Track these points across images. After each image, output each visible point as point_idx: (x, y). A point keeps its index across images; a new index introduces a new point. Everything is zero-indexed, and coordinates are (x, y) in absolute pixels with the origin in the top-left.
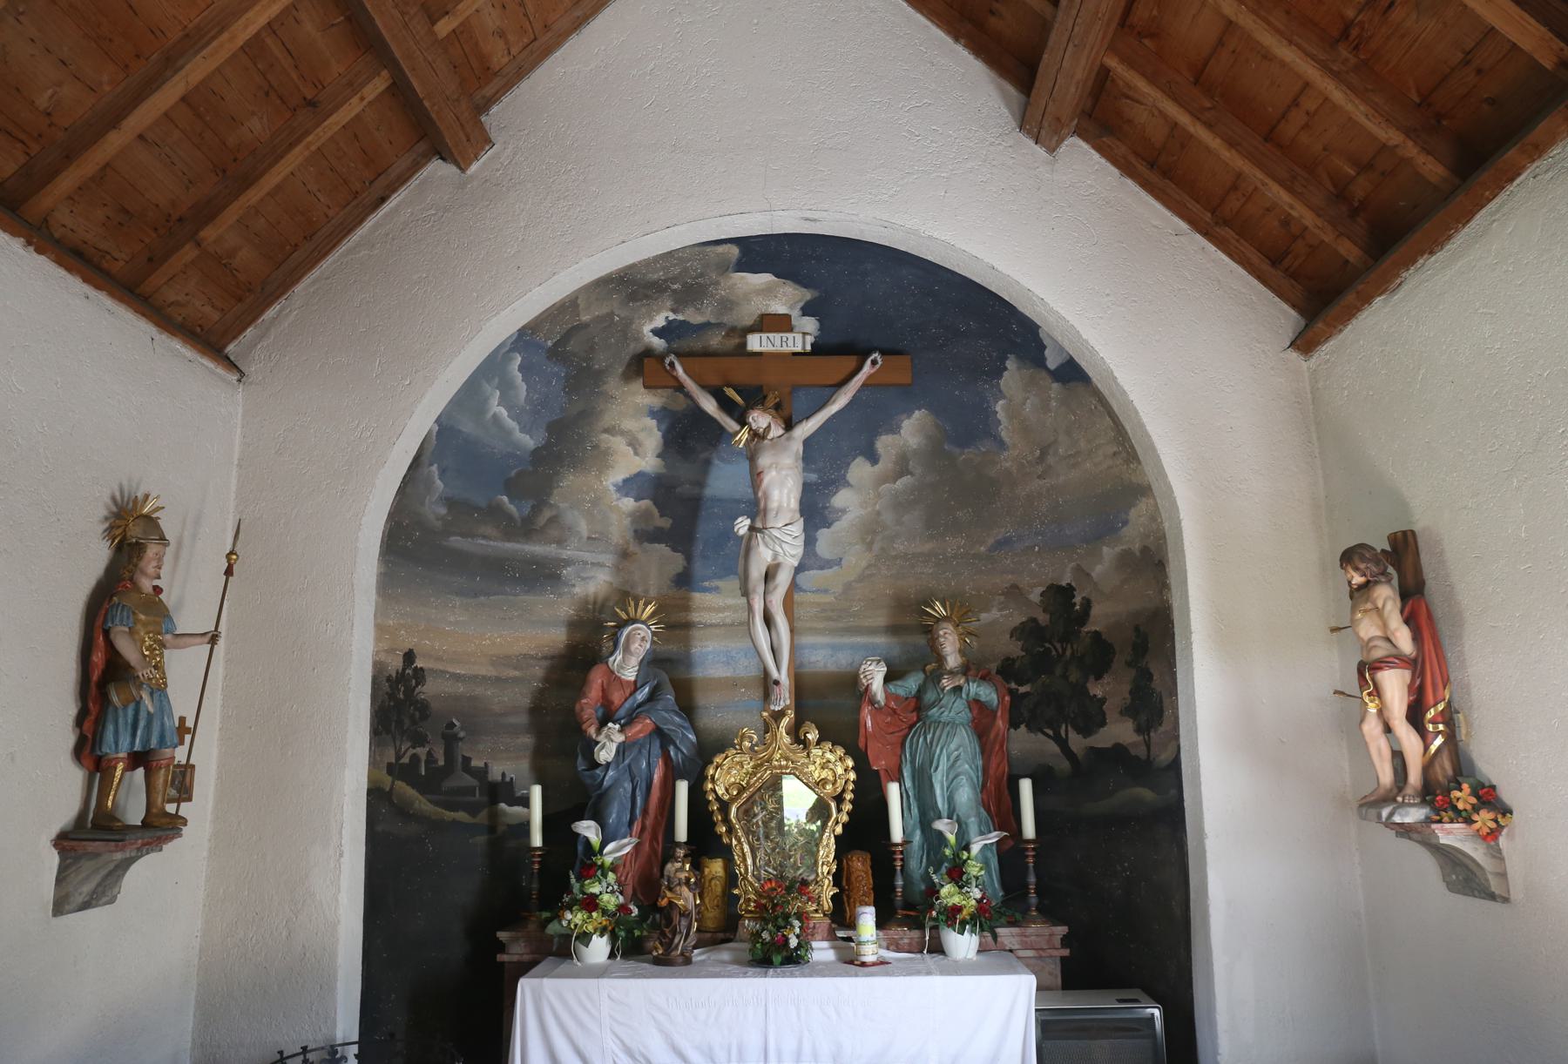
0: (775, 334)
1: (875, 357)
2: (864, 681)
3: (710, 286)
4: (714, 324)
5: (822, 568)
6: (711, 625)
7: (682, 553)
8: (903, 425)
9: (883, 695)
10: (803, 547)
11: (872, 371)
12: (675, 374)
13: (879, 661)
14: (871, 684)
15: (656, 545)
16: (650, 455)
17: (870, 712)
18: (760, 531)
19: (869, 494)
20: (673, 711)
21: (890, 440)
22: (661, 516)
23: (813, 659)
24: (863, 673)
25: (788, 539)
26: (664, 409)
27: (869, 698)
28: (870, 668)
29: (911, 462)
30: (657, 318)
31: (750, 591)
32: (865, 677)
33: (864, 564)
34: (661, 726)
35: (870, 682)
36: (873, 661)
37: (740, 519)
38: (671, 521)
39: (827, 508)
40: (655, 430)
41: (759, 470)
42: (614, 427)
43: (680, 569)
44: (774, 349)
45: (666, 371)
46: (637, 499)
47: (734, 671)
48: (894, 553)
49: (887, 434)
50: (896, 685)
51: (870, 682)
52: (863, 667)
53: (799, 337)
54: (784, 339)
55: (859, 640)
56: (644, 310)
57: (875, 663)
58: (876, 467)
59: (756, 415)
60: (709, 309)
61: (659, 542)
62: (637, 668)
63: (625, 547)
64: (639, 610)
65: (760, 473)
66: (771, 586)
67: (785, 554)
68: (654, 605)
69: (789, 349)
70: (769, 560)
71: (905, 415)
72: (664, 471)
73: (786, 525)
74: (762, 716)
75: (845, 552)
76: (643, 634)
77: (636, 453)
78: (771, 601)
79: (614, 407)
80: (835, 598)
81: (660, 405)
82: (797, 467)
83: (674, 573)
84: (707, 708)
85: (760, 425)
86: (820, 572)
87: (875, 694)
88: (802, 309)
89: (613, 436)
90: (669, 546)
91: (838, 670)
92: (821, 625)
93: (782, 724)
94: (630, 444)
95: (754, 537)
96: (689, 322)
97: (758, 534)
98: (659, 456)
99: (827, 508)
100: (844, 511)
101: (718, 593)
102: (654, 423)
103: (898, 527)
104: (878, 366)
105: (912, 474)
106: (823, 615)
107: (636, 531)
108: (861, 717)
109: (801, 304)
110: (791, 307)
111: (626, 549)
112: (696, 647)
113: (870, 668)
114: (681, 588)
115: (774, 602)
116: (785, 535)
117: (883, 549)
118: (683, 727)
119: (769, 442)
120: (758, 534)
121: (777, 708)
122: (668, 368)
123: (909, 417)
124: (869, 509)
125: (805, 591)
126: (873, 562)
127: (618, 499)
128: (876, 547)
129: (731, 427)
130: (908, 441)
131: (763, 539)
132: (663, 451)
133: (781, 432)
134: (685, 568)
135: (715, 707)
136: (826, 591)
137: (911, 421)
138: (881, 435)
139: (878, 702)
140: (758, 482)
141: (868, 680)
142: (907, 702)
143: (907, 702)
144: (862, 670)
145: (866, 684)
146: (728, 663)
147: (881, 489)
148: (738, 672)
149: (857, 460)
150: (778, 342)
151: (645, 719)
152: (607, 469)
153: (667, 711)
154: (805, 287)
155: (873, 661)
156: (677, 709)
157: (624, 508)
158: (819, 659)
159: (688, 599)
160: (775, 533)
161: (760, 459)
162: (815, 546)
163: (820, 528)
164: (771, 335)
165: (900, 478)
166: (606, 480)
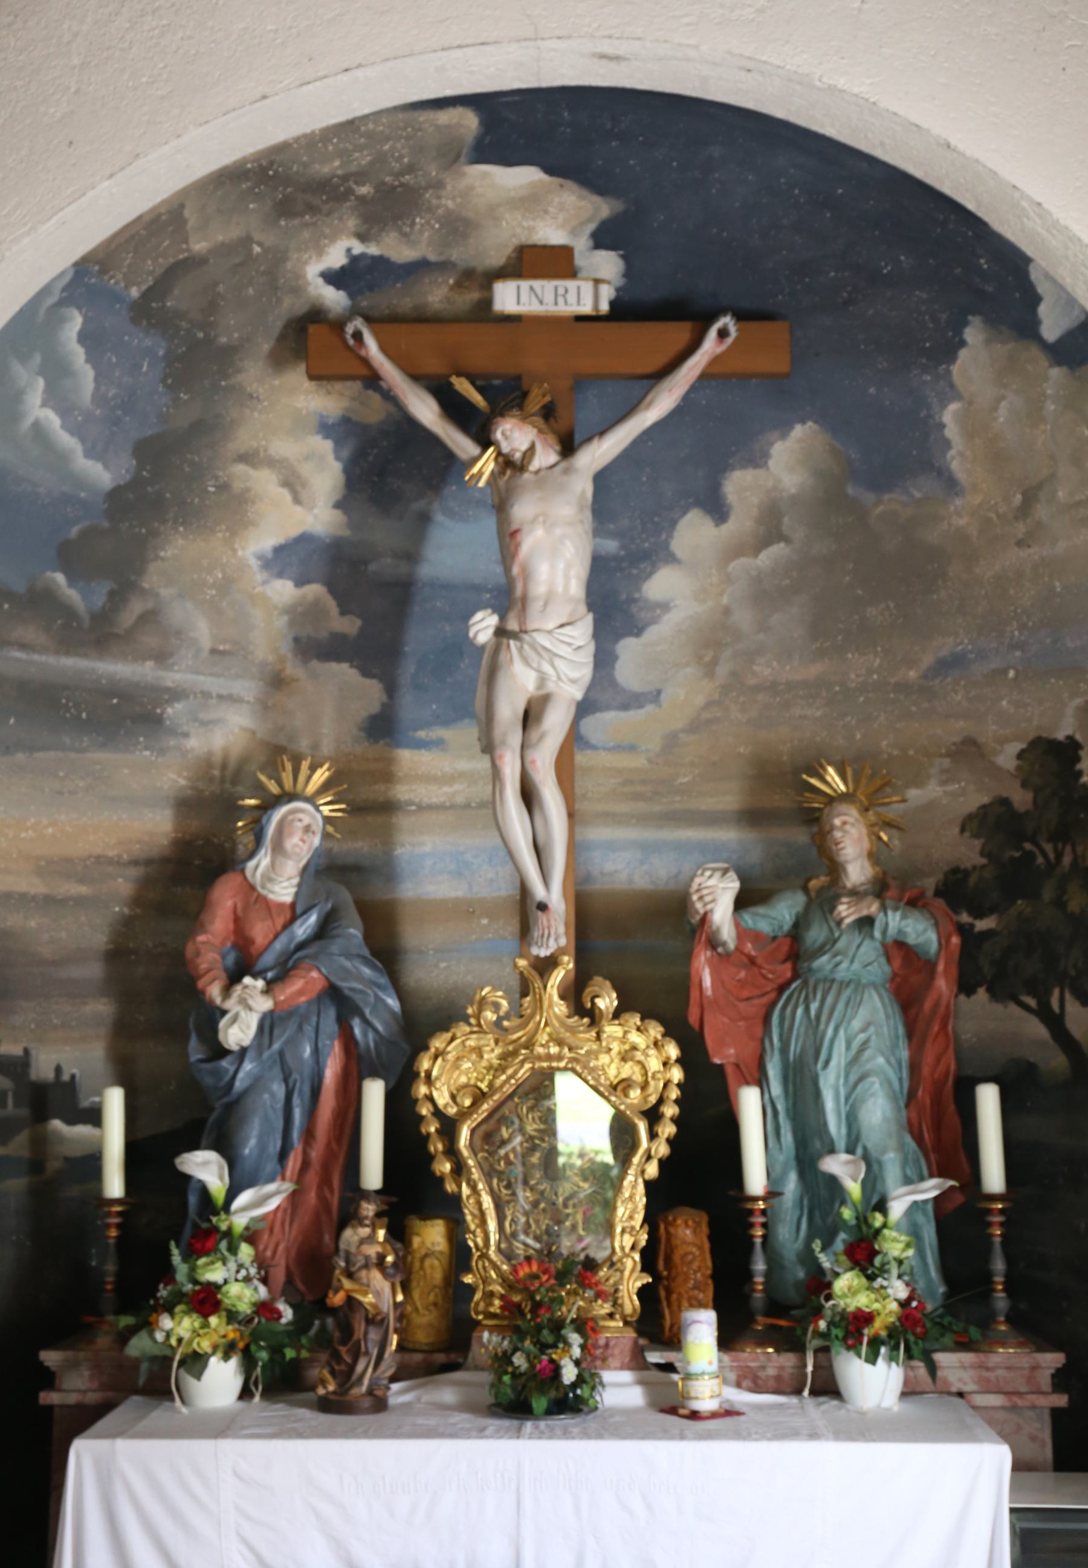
2: (699, 906)
3: (426, 189)
5: (625, 707)
6: (431, 808)
7: (381, 680)
12: (363, 353)
13: (725, 872)
14: (711, 911)
22: (343, 613)
23: (609, 867)
24: (698, 890)
25: (563, 650)
26: (346, 421)
29: (786, 520)
32: (701, 898)
33: (700, 700)
37: (479, 616)
38: (358, 623)
40: (331, 458)
41: (514, 527)
42: (256, 453)
43: (375, 708)
46: (299, 583)
48: (752, 682)
49: (743, 467)
50: (757, 914)
51: (709, 907)
52: (697, 880)
54: (561, 291)
56: (306, 234)
57: (718, 874)
60: (426, 234)
64: (302, 778)
66: (534, 735)
67: (559, 678)
68: (329, 769)
73: (562, 626)
74: (515, 966)
76: (307, 820)
77: (297, 500)
79: (256, 414)
80: (650, 761)
83: (364, 714)
86: (623, 715)
87: (718, 930)
89: (254, 466)
90: (356, 667)
92: (622, 808)
94: (287, 484)
95: (504, 647)
97: (512, 642)
98: (338, 505)
99: (635, 601)
100: (665, 607)
102: (326, 446)
103: (761, 636)
104: (729, 341)
107: (297, 640)
109: (592, 227)
110: (574, 232)
115: (539, 763)
117: (733, 674)
118: (379, 986)
121: (543, 953)
122: (351, 342)
123: (784, 436)
124: (710, 603)
125: (594, 748)
126: (716, 697)
131: (520, 650)
133: (553, 457)
134: (384, 705)
135: (436, 951)
136: (632, 748)
139: (724, 944)
140: (512, 548)
141: (705, 905)
142: (774, 945)
143: (774, 945)
145: (702, 911)
150: (549, 297)
151: (310, 970)
153: (348, 956)
155: (714, 870)
156: (366, 952)
159: (390, 761)
160: (542, 640)
162: (613, 668)
164: (537, 284)
166: (243, 548)
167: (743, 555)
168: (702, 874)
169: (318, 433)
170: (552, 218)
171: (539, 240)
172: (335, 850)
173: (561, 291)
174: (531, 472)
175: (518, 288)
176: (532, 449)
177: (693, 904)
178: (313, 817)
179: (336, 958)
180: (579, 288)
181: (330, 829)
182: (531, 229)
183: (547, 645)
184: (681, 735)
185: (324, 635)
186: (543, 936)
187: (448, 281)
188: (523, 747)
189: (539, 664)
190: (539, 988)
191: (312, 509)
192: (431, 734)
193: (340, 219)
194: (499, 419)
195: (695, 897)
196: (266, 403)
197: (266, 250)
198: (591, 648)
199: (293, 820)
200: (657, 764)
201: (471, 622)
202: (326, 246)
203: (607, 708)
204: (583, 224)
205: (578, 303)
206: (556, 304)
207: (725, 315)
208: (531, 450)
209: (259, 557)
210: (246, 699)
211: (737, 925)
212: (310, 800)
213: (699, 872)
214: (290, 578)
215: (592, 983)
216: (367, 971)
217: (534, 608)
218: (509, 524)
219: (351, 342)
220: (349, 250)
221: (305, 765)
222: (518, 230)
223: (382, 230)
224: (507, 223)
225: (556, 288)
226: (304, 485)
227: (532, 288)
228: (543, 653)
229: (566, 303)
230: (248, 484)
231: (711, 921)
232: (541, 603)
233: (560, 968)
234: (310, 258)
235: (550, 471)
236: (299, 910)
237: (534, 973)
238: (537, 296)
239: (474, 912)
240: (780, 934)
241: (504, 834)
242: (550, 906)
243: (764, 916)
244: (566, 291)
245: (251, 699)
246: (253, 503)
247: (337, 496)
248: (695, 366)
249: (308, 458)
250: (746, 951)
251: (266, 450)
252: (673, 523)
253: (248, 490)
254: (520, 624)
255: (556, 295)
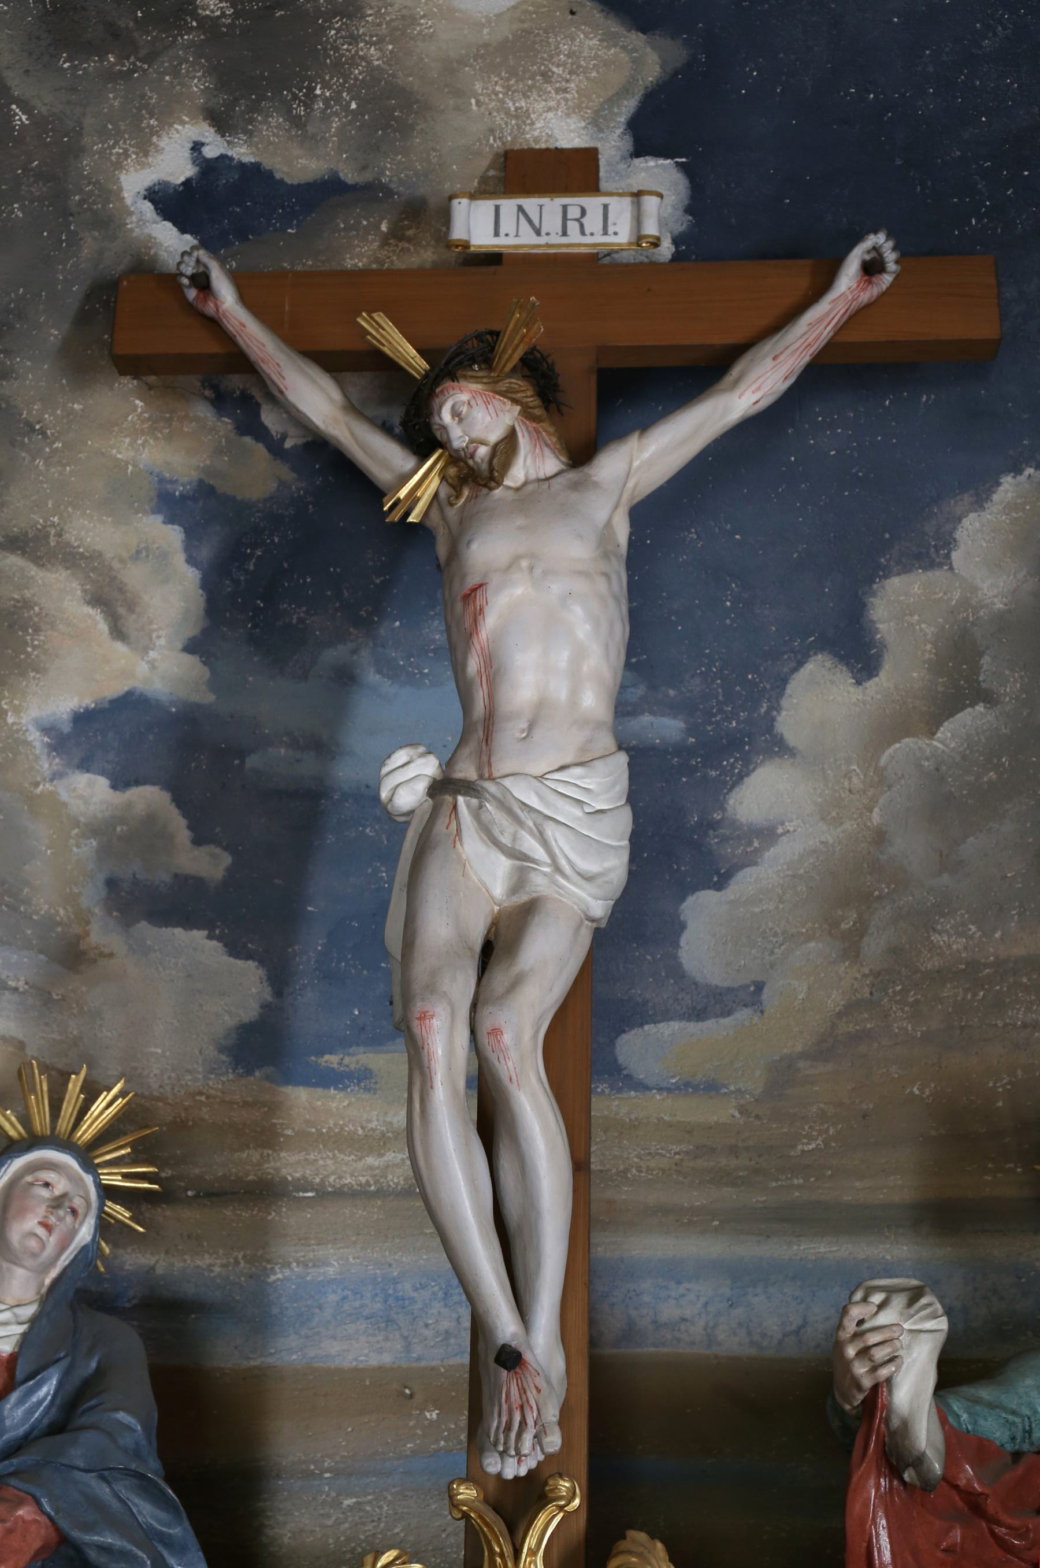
0: (545, 201)
1: (875, 249)
2: (860, 1369)
3: (329, 16)
4: (354, 188)
5: (698, 1014)
6: (341, 1194)
7: (262, 963)
8: (960, 534)
9: (939, 1438)
10: (625, 857)
11: (865, 297)
12: (210, 309)
13: (915, 1295)
14: (889, 1381)
15: (178, 931)
16: (162, 642)
17: (887, 1501)
18: (468, 788)
19: (847, 775)
20: (128, 1472)
21: (916, 589)
22: (197, 842)
23: (669, 1312)
24: (857, 1336)
25: (567, 813)
26: (205, 491)
27: (882, 1445)
28: (883, 1319)
29: (986, 660)
30: (163, 142)
31: (417, 987)
32: (864, 1352)
33: (835, 1000)
34: (76, 1534)
35: (884, 1372)
36: (891, 1291)
37: (401, 757)
38: (227, 859)
39: (714, 825)
40: (179, 559)
41: (471, 581)
42: (42, 536)
43: (250, 1012)
44: (542, 240)
45: (190, 308)
46: (119, 783)
47: (408, 1348)
48: (933, 963)
49: (906, 570)
50: (977, 1401)
51: (884, 1372)
52: (856, 1312)
53: (621, 210)
54: (574, 213)
55: (823, 1249)
56: (114, 100)
57: (899, 1301)
58: (872, 684)
59: (464, 397)
60: (335, 124)
61: (188, 922)
62: (29, 1311)
63: (75, 929)
64: (68, 1110)
65: (475, 590)
66: (499, 979)
67: (558, 869)
68: (122, 1094)
69: (588, 240)
70: (499, 890)
71: (967, 498)
72: (210, 698)
73: (562, 768)
74: (454, 1504)
75: (772, 966)
76: (61, 1185)
77: (118, 633)
78: (496, 1032)
79: (40, 463)
80: (743, 1110)
81: (195, 475)
82: (606, 575)
83: (230, 1021)
84: (309, 1475)
85: (477, 433)
86: (693, 1027)
87: (906, 1426)
88: (634, 125)
89: (38, 561)
90: (219, 939)
91: (752, 1352)
92: (696, 1198)
93: (530, 1541)
94: (97, 600)
95: (446, 809)
96: (269, 175)
97: (461, 799)
98: (191, 647)
99: (714, 825)
100: (768, 834)
101: (367, 1090)
102: (173, 536)
103: (945, 879)
104: (886, 280)
105: (988, 698)
106: (700, 1163)
107: (112, 883)
108: (851, 1524)
109: (629, 106)
110: (597, 122)
111: (79, 938)
112: (287, 1265)
113: (883, 1319)
114: (249, 1072)
115: (507, 1038)
116: (561, 803)
117: (894, 951)
118: (167, 1541)
119: (510, 495)
120: (461, 799)
121: (512, 1469)
122: (192, 294)
123: (980, 502)
124: (849, 826)
125: (642, 1087)
126: (866, 993)
127: (56, 776)
128: (874, 946)
129: (385, 464)
130: (975, 589)
131: (477, 814)
132: (205, 632)
133: (551, 464)
134: (265, 1006)
135: (337, 1473)
136: (712, 1088)
137: (986, 516)
138: (886, 577)
139: (919, 1462)
140: (468, 623)
141: (874, 1369)
142: (1020, 1470)
143: (1020, 1470)
144: (850, 1327)
145: (867, 1383)
146: (389, 1321)
147: (883, 760)
148: (417, 1350)
149: (809, 667)
150: (552, 222)
151: (20, 1503)
152: (23, 674)
153: (105, 1474)
154: (644, 31)
155: (891, 1291)
156: (153, 1467)
157: (76, 807)
158: (688, 1313)
159: (273, 1107)
160: (523, 792)
161: (474, 546)
162: (676, 945)
163: (695, 889)
164: (531, 204)
165: (951, 715)
166: (17, 710)
167: (908, 734)
168: (865, 1300)
169: (155, 511)
170: (558, 91)
171: (537, 140)
172: (160, 1271)
173: (574, 213)
174: (509, 488)
175: (497, 209)
176: (510, 440)
177: (847, 1364)
178: (78, 1182)
179: (78, 1475)
180: (606, 207)
181: (120, 1212)
182: (522, 116)
183: (534, 802)
184: (801, 1064)
185: (164, 877)
186: (508, 1428)
187: (378, 228)
188: (474, 1006)
189: (515, 838)
190: (502, 1555)
191: (146, 650)
192: (347, 1060)
193: (175, 72)
194: (448, 384)
195: (851, 1351)
196: (58, 445)
197: (39, 123)
198: (624, 820)
199: (32, 1184)
200: (757, 1117)
201: (385, 770)
202: (154, 132)
203: (665, 1015)
204: (612, 101)
205: (605, 232)
206: (565, 233)
207: (876, 232)
208: (508, 445)
209: (48, 729)
210: (12, 983)
211: (943, 1415)
212: (86, 1154)
213: (859, 1296)
214: (103, 773)
215: (622, 1545)
216: (147, 1512)
217: (508, 735)
218: (463, 577)
219: (192, 294)
220: (197, 147)
221: (75, 1084)
222: (499, 119)
223: (254, 108)
224: (478, 103)
225: (565, 208)
226: (131, 606)
227: (520, 209)
228: (523, 815)
229: (583, 232)
230: (27, 594)
231: (888, 1407)
232: (524, 725)
233: (551, 1508)
234: (126, 154)
235: (545, 485)
236: (20, 1374)
237: (491, 1516)
238: (530, 221)
239: (411, 1396)
240: (1026, 1447)
241: (433, 1203)
242: (527, 1356)
243: (992, 1406)
244: (583, 212)
245: (21, 985)
246: (37, 630)
247: (192, 630)
248: (820, 320)
249: (137, 556)
250: (962, 1482)
251: (59, 535)
252: (781, 683)
253: (27, 604)
254: (479, 769)
255: (565, 219)
